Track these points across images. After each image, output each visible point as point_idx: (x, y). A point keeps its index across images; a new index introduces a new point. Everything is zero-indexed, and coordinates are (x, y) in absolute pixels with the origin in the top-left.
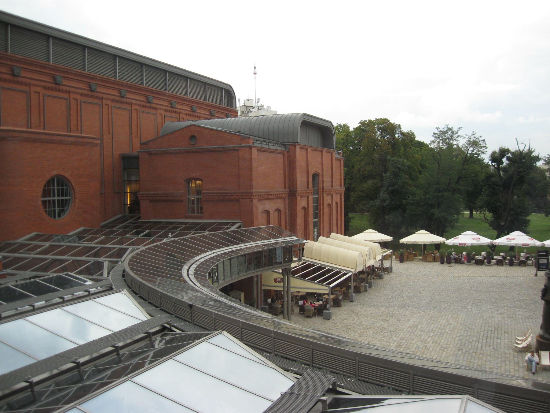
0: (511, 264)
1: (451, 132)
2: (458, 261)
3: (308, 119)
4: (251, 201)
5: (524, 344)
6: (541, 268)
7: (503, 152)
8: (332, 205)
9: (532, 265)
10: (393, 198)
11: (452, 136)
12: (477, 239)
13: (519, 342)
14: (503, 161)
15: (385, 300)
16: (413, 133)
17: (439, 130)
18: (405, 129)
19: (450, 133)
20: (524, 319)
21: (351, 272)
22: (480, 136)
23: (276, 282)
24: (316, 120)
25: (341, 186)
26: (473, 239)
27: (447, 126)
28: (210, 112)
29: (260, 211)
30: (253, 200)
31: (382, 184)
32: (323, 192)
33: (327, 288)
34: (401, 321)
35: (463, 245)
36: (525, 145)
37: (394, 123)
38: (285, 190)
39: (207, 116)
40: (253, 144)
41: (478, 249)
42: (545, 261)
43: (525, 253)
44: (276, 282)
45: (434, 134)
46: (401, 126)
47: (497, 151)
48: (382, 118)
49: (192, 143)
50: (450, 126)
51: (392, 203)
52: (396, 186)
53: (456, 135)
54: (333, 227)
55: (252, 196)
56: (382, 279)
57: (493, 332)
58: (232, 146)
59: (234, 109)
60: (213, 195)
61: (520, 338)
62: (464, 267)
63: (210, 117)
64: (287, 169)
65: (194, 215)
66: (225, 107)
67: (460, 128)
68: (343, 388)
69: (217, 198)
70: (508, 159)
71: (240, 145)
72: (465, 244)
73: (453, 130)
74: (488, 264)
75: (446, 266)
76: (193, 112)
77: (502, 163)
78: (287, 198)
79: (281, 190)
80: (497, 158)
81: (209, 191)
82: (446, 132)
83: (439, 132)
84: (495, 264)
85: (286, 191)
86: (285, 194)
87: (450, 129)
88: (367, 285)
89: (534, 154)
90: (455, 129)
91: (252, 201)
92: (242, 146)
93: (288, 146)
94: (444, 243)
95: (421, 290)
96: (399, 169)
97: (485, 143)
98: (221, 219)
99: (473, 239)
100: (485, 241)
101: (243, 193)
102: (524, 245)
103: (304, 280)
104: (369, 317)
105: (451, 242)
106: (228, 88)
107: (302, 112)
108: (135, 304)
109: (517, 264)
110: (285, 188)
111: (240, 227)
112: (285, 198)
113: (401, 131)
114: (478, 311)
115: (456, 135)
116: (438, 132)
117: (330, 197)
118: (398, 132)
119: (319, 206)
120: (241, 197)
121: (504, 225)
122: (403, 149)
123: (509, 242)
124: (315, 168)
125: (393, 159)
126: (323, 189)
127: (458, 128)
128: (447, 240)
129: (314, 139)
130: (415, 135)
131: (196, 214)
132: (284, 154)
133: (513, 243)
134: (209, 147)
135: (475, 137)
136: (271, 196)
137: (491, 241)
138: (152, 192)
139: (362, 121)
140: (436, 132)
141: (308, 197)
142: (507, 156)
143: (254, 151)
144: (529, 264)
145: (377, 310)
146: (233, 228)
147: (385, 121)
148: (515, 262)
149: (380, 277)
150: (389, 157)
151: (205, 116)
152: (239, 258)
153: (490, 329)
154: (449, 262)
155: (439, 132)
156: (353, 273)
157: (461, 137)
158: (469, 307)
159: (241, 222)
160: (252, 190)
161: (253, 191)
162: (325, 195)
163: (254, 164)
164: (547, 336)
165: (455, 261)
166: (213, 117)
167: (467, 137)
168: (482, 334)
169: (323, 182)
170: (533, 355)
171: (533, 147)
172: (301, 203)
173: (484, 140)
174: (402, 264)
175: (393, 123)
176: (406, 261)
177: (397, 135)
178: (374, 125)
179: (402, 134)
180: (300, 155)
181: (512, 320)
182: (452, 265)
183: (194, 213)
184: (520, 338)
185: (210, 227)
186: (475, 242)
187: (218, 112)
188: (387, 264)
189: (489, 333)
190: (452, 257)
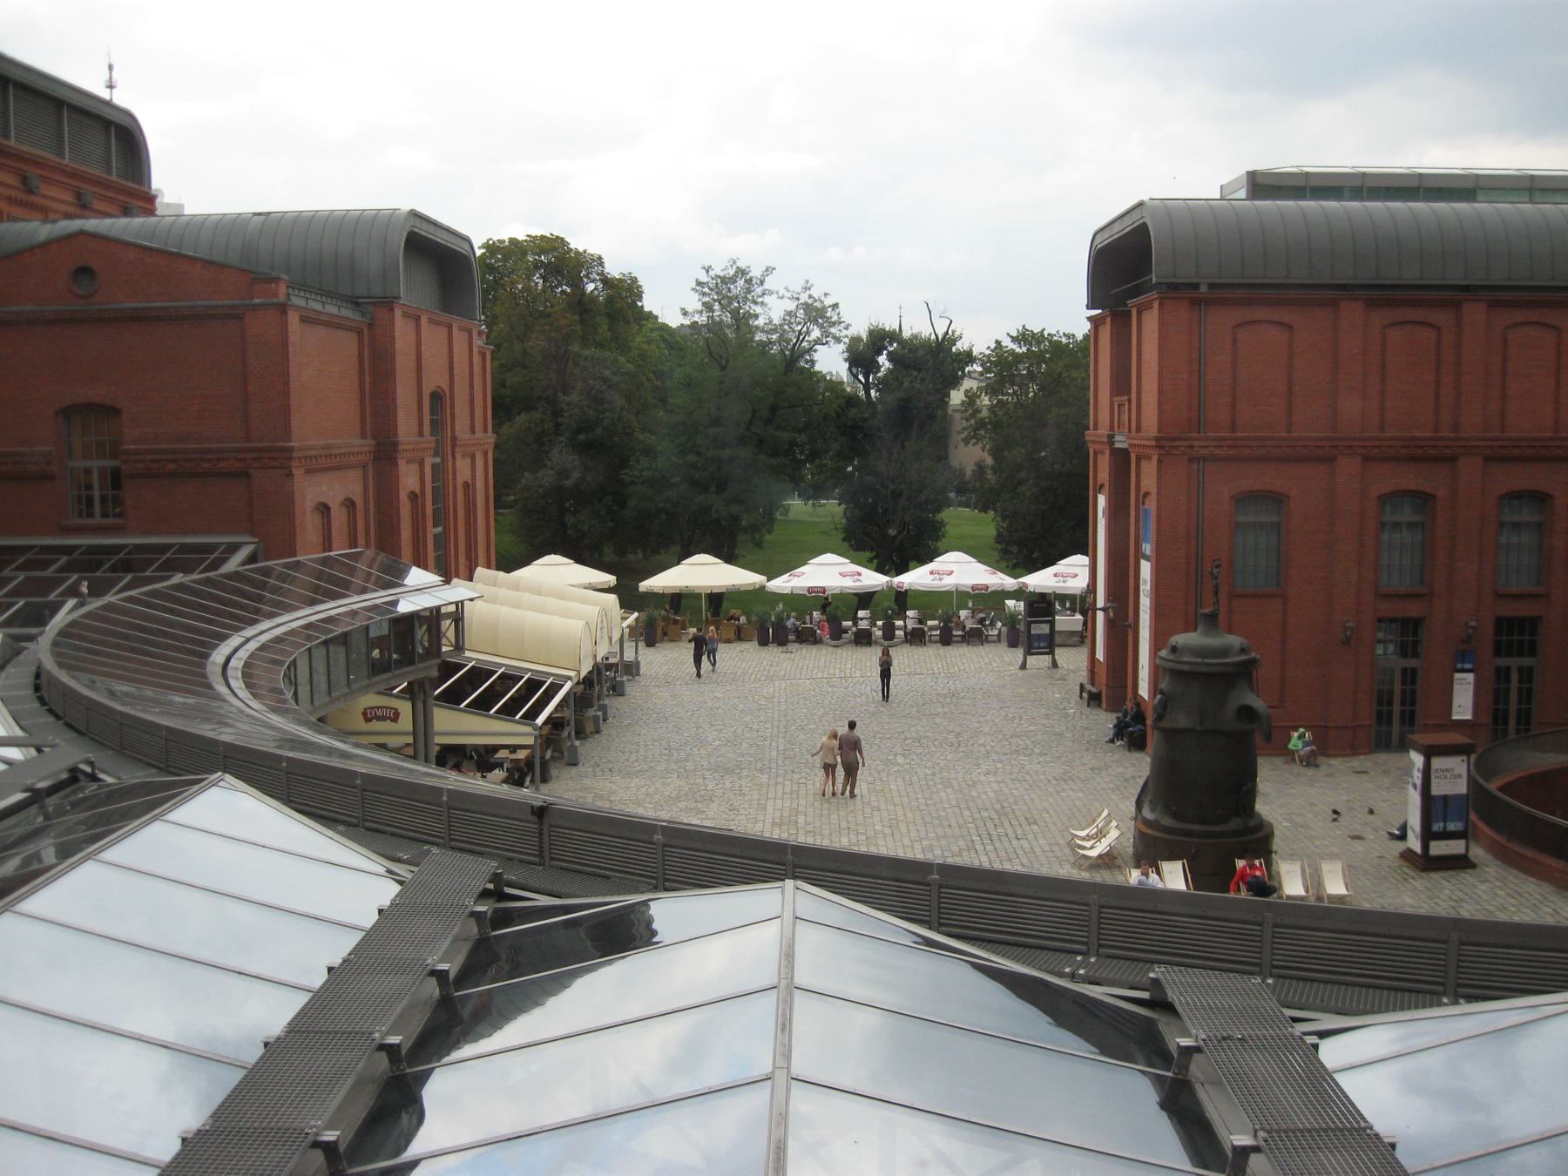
0: (946, 639)
1: (746, 281)
2: (807, 637)
3: (425, 231)
4: (287, 475)
5: (1101, 848)
6: (1036, 648)
7: (879, 339)
8: (474, 484)
9: (999, 640)
10: (589, 464)
11: (749, 291)
12: (852, 575)
13: (1088, 844)
14: (881, 364)
15: (665, 755)
16: (634, 280)
17: (712, 273)
18: (613, 269)
19: (741, 283)
20: (1054, 782)
21: (569, 678)
22: (826, 294)
23: (368, 720)
24: (439, 232)
25: (421, 434)
26: (843, 575)
27: (735, 262)
28: (79, 196)
29: (309, 504)
30: (294, 470)
31: (558, 425)
32: (453, 446)
33: (528, 729)
34: (742, 811)
35: (818, 592)
36: (951, 322)
37: (585, 251)
38: (364, 442)
39: (71, 209)
40: (289, 299)
41: (988, 600)
42: (1045, 629)
43: (969, 609)
44: (368, 720)
45: (699, 283)
46: (605, 260)
47: (864, 336)
48: (548, 235)
49: (79, 291)
50: (742, 264)
51: (589, 479)
52: (599, 431)
53: (759, 290)
54: (476, 550)
55: (290, 459)
56: (622, 695)
57: (997, 822)
58: (220, 303)
59: (146, 189)
60: (158, 456)
61: (1083, 834)
62: (824, 652)
63: (79, 211)
64: (368, 379)
65: (90, 521)
66: (117, 180)
67: (769, 270)
68: (1302, 1009)
69: (171, 466)
70: (891, 357)
71: (247, 302)
72: (987, 588)
73: (751, 274)
74: (833, 643)
75: (773, 653)
76: (30, 191)
77: (879, 368)
78: (370, 467)
79: (358, 444)
80: (861, 356)
81: (144, 446)
82: (733, 280)
83: (713, 279)
84: (850, 642)
85: (368, 446)
86: (365, 453)
87: (742, 272)
88: (600, 713)
89: (961, 346)
90: (756, 272)
91: (290, 475)
92: (253, 305)
93: (370, 308)
94: (763, 587)
95: (748, 719)
96: (605, 380)
97: (839, 314)
98: (187, 533)
99: (843, 575)
100: (872, 579)
101: (261, 450)
102: (978, 589)
103: (455, 709)
104: (648, 805)
105: (782, 584)
106: (125, 122)
107: (405, 206)
108: (278, 808)
109: (960, 639)
110: (363, 435)
111: (252, 559)
112: (364, 467)
113: (602, 274)
114: (929, 768)
115: (759, 290)
116: (709, 279)
117: (468, 461)
118: (594, 276)
119: (444, 487)
120: (256, 464)
121: (896, 536)
122: (605, 327)
123: (938, 582)
124: (434, 379)
125: (587, 352)
126: (454, 438)
127: (764, 269)
128: (768, 580)
129: (414, 290)
130: (640, 286)
131: (97, 519)
132: (359, 332)
133: (948, 582)
134: (141, 305)
135: (810, 297)
136: (334, 460)
137: (887, 578)
138: (132, 447)
139: (491, 242)
140: (704, 278)
141: (422, 463)
142: (891, 349)
143: (293, 318)
144: (990, 638)
145: (658, 785)
146: (233, 564)
147: (554, 245)
148: (955, 633)
149: (617, 690)
150: (575, 348)
151: (63, 208)
152: (313, 650)
153: (985, 814)
154: (781, 641)
155: (713, 279)
156: (575, 680)
157: (771, 293)
158: (900, 760)
159: (256, 540)
160: (291, 441)
161: (293, 444)
162: (458, 456)
163: (295, 359)
164: (1167, 821)
165: (798, 637)
166: (88, 213)
167: (789, 295)
168: (973, 831)
169: (453, 416)
170: (1146, 874)
171: (957, 328)
172: (408, 480)
173: (837, 304)
174: (652, 649)
175: (581, 251)
176: (662, 641)
177: (590, 287)
178: (524, 253)
179: (607, 281)
180: (402, 329)
181: (1028, 787)
182: (791, 647)
183: (90, 515)
184: (1083, 834)
185: (159, 559)
186: (848, 584)
187: (103, 198)
188: (629, 655)
189: (990, 825)
190: (789, 624)
